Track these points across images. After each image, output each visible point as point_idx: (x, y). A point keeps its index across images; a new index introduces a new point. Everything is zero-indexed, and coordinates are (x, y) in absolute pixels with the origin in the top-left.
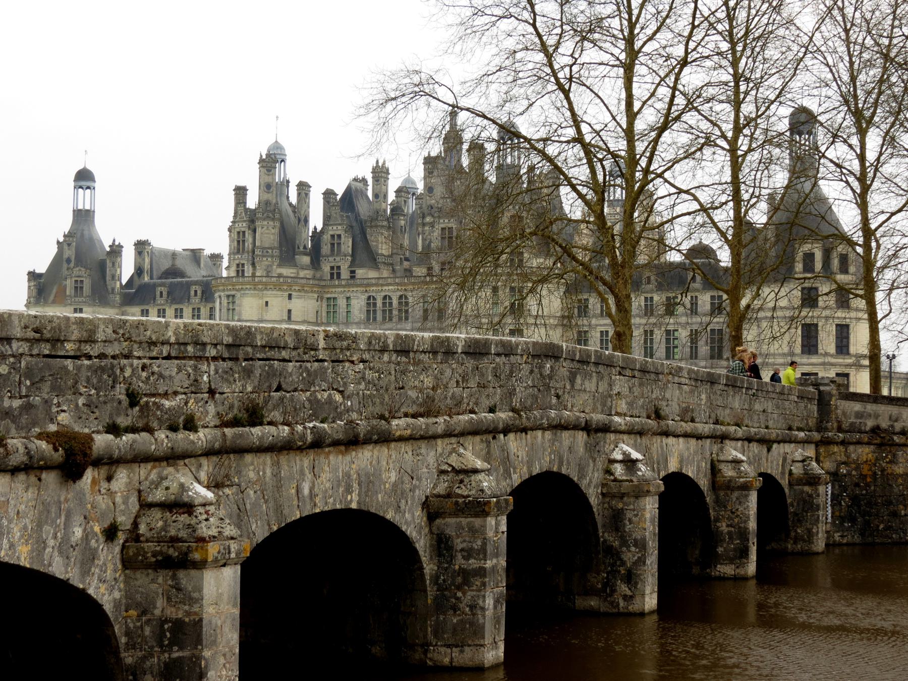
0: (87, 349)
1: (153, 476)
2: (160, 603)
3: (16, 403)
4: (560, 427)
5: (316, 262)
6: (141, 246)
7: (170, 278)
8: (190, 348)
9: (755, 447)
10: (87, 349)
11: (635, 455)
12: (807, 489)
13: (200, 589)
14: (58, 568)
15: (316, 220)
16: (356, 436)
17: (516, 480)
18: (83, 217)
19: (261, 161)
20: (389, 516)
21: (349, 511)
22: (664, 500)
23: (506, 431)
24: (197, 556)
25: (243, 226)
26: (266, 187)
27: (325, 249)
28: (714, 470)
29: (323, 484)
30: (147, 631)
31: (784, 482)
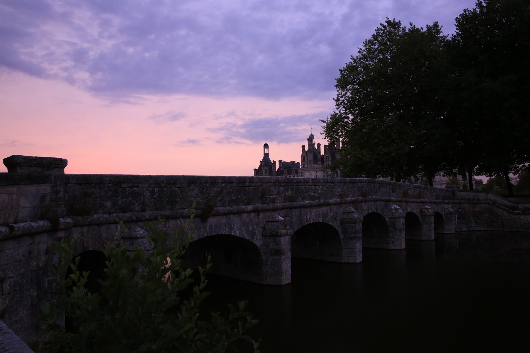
0: (252, 184)
1: (269, 214)
2: (271, 245)
3: (235, 198)
4: (376, 200)
5: (323, 163)
6: (280, 161)
7: (288, 167)
8: (277, 184)
9: (433, 205)
10: (252, 184)
11: (398, 207)
12: (449, 216)
13: (280, 241)
14: (246, 237)
15: (322, 152)
16: (166, 219)
17: (365, 214)
18: (266, 156)
19: (308, 139)
20: (331, 224)
21: (319, 223)
22: (406, 219)
23: (361, 202)
24: (279, 234)
25: (304, 155)
26: (309, 145)
27: (325, 160)
28: (421, 212)
29: (312, 216)
30: (268, 252)
31: (443, 214)
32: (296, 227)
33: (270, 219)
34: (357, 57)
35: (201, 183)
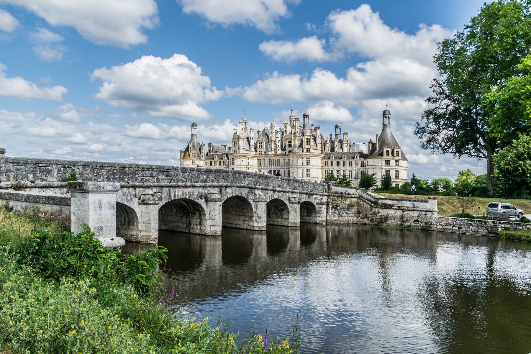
29: (179, 194)
32: (164, 201)
33: (144, 193)
34: (511, 77)
35: (93, 166)
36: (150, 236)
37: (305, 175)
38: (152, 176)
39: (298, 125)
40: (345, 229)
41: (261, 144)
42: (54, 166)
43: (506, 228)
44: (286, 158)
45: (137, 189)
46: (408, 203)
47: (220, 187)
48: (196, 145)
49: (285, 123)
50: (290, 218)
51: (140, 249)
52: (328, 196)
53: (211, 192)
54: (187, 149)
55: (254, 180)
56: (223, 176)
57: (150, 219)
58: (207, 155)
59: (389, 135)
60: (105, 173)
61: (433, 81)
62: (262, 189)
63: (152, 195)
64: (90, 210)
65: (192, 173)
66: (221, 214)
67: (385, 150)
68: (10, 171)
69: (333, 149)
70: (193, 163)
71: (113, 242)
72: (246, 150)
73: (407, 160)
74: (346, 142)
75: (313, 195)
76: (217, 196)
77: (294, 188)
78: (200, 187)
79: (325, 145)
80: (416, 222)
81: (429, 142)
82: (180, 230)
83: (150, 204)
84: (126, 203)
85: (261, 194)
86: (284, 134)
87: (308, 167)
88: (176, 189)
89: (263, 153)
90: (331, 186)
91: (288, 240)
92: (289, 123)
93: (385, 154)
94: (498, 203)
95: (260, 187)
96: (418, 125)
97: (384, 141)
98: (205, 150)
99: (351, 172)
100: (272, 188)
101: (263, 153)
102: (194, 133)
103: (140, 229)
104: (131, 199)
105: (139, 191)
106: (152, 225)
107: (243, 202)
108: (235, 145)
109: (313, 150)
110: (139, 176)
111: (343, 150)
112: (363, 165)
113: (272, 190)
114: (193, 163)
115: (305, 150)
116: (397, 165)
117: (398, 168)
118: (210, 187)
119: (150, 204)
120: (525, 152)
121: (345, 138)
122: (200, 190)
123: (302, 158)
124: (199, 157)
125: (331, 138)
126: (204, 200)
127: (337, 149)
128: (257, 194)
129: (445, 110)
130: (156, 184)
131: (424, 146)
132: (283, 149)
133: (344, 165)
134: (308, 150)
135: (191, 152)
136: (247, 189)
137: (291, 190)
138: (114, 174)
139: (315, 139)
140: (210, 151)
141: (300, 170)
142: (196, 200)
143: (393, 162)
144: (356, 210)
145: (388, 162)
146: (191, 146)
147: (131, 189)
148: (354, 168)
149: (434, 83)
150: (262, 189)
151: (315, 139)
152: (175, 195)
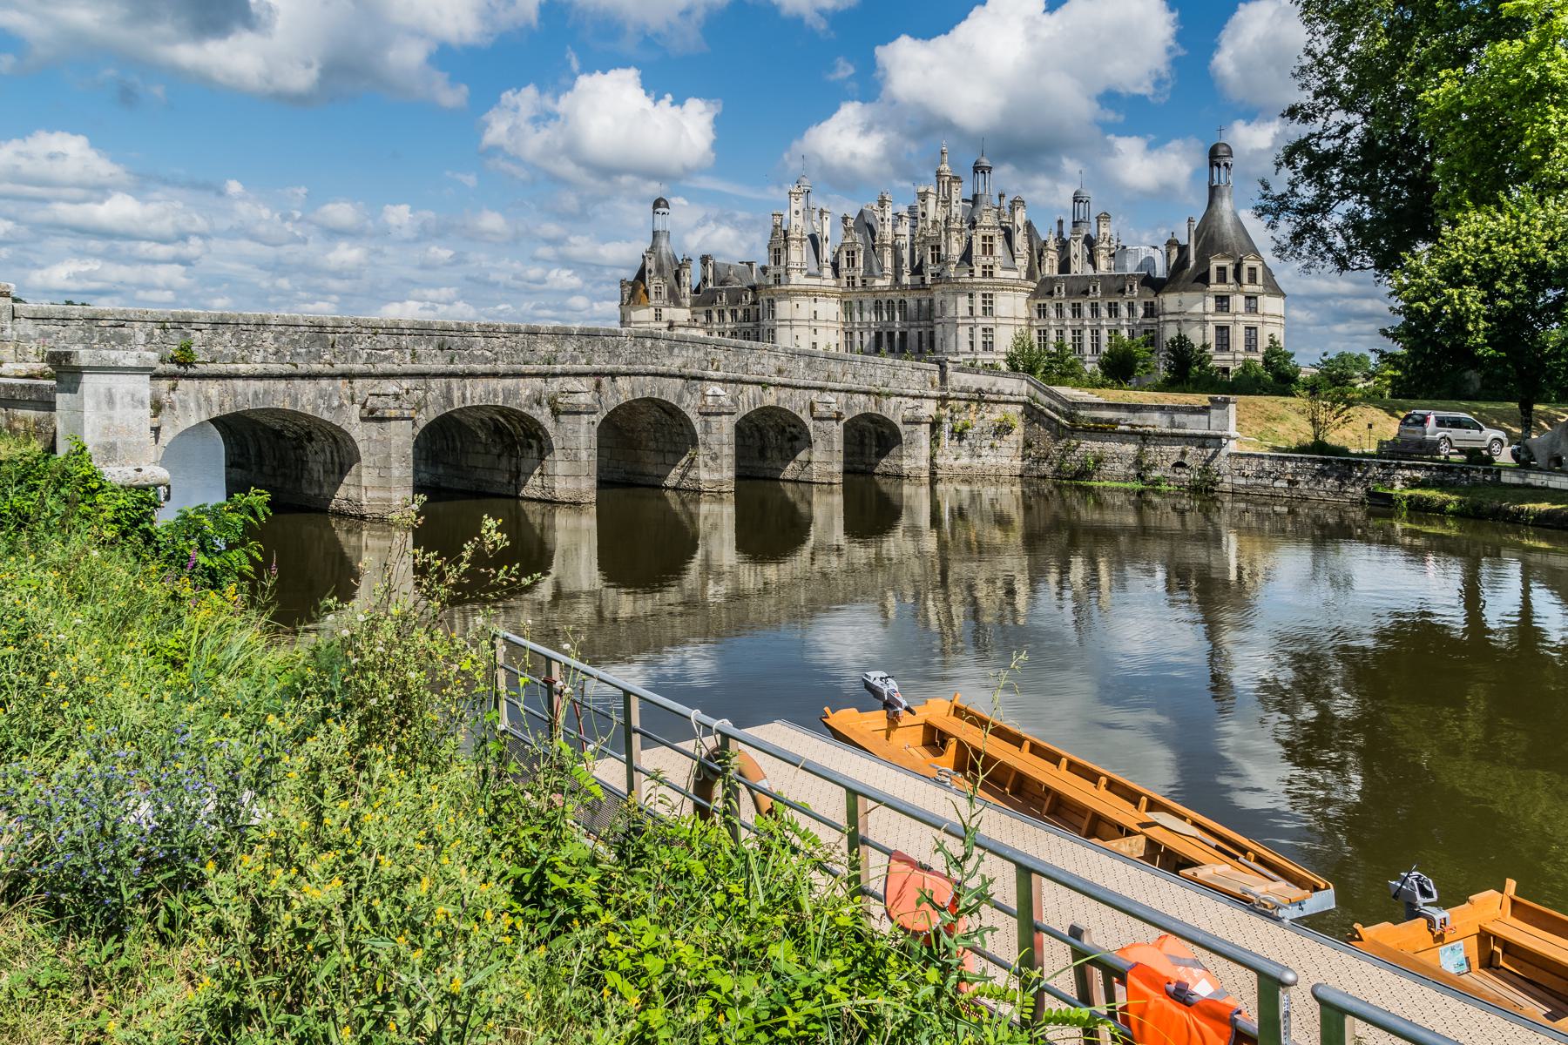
32: (432, 413)
33: (376, 391)
36: (389, 500)
37: (979, 346)
38: (398, 348)
39: (958, 192)
40: (988, 492)
41: (851, 253)
42: (137, 324)
43: (1416, 479)
44: (922, 295)
45: (358, 383)
46: (1156, 415)
47: (595, 374)
48: (665, 261)
49: (922, 189)
50: (814, 459)
51: (365, 533)
52: (943, 400)
53: (569, 387)
54: (641, 275)
55: (701, 354)
56: (604, 345)
57: (389, 456)
58: (697, 291)
59: (1228, 220)
60: (270, 340)
61: (1302, 55)
62: (724, 381)
63: (397, 396)
64: (87, 407)
65: (514, 338)
66: (594, 445)
67: (1214, 264)
68: (28, 338)
69: (1064, 266)
70: (658, 317)
71: (140, 475)
72: (809, 275)
73: (1282, 295)
74: (1105, 245)
75: (888, 396)
76: (584, 399)
77: (828, 378)
78: (537, 375)
79: (1041, 255)
80: (1178, 470)
81: (1297, 238)
82: (495, 490)
83: (390, 419)
84: (326, 416)
85: (720, 392)
86: (920, 225)
87: (988, 321)
88: (468, 381)
89: (858, 283)
90: (949, 372)
91: (811, 518)
92: (932, 189)
93: (1213, 277)
94: (1424, 412)
95: (720, 374)
96: (1267, 188)
97: (1213, 239)
98: (692, 276)
99: (1078, 334)
100: (755, 378)
101: (858, 283)
102: (659, 227)
103: (365, 482)
104: (341, 406)
105: (364, 386)
106: (396, 473)
107: (670, 414)
108: (777, 261)
109: (1003, 268)
110: (363, 345)
111: (1095, 268)
112: (1150, 311)
113: (758, 383)
114: (658, 317)
115: (978, 271)
116: (1252, 308)
117: (1253, 319)
118: (565, 374)
119: (390, 419)
120: (1467, 262)
121: (1102, 230)
122: (538, 382)
123: (971, 296)
124: (675, 299)
125: (1060, 233)
126: (547, 410)
127: (1079, 267)
128: (710, 392)
129: (1338, 142)
130: (409, 367)
131: (1283, 250)
132: (917, 270)
133: (1095, 310)
134: (988, 272)
135: (653, 283)
136: (679, 382)
137: (819, 383)
138: (294, 342)
139: (1008, 236)
140: (705, 280)
141: (963, 332)
142: (525, 410)
143: (1238, 303)
144: (1021, 438)
145: (1222, 302)
146: (651, 265)
147: (340, 382)
148: (1124, 322)
149: (1308, 61)
150: (724, 381)
151: (1008, 236)
152: (464, 395)
